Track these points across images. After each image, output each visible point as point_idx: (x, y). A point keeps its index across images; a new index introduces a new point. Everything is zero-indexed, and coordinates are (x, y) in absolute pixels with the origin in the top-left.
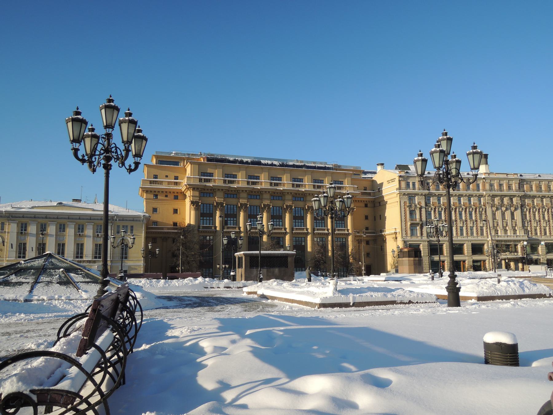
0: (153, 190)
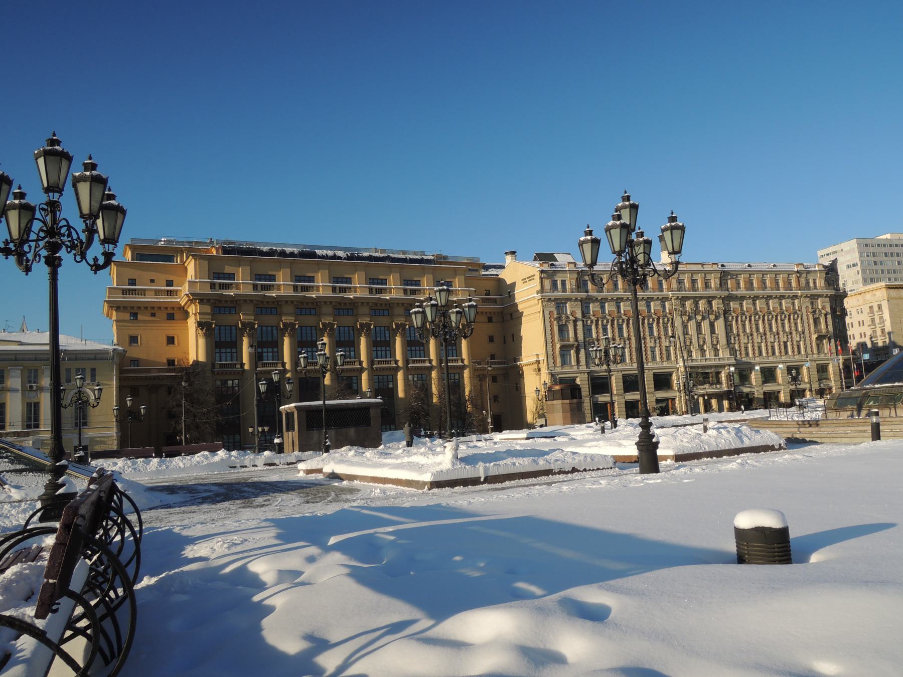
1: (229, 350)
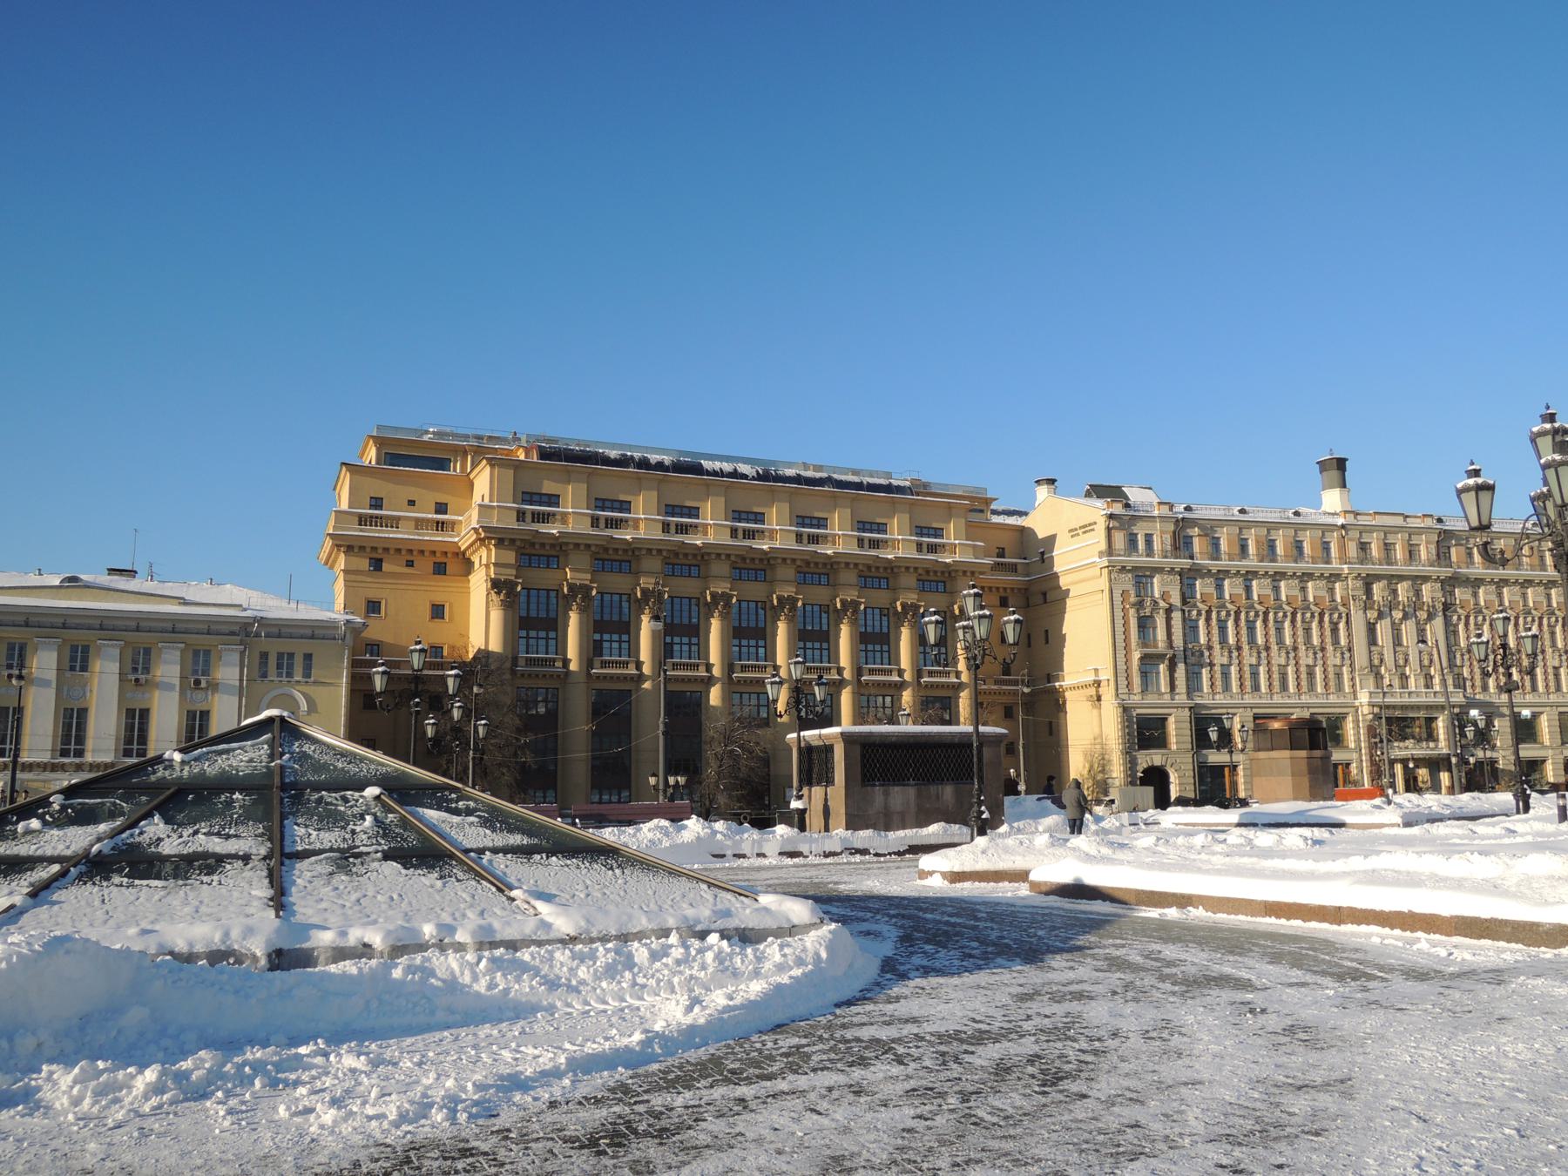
0: (368, 544)
1: (542, 634)
